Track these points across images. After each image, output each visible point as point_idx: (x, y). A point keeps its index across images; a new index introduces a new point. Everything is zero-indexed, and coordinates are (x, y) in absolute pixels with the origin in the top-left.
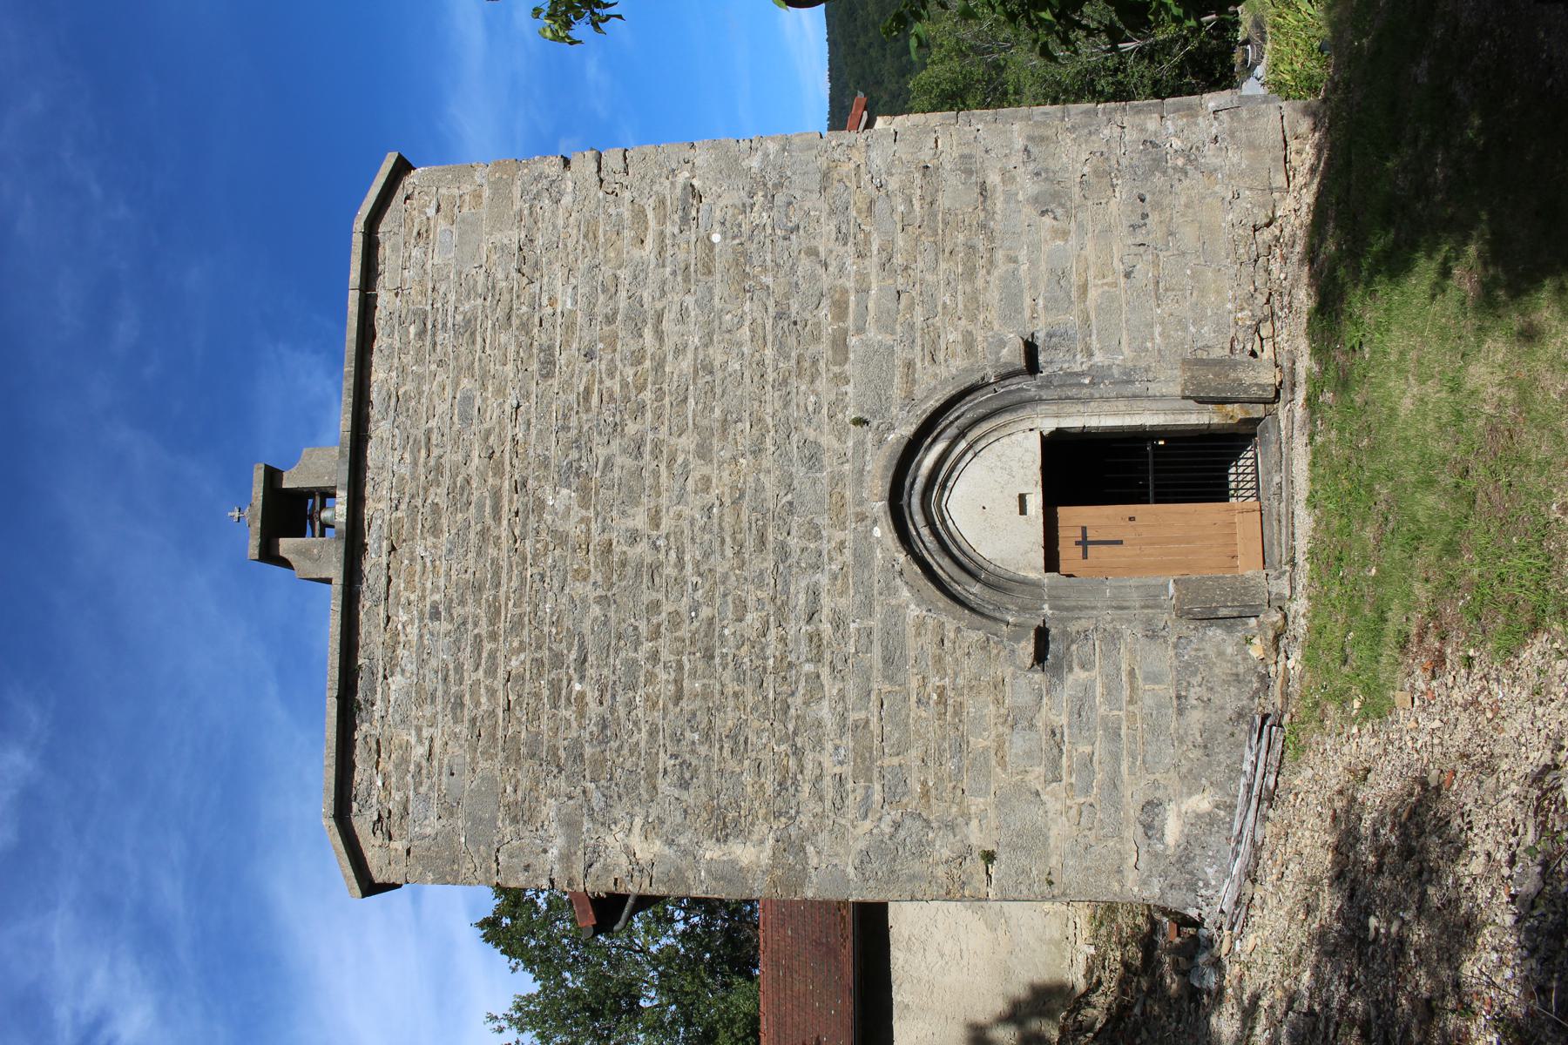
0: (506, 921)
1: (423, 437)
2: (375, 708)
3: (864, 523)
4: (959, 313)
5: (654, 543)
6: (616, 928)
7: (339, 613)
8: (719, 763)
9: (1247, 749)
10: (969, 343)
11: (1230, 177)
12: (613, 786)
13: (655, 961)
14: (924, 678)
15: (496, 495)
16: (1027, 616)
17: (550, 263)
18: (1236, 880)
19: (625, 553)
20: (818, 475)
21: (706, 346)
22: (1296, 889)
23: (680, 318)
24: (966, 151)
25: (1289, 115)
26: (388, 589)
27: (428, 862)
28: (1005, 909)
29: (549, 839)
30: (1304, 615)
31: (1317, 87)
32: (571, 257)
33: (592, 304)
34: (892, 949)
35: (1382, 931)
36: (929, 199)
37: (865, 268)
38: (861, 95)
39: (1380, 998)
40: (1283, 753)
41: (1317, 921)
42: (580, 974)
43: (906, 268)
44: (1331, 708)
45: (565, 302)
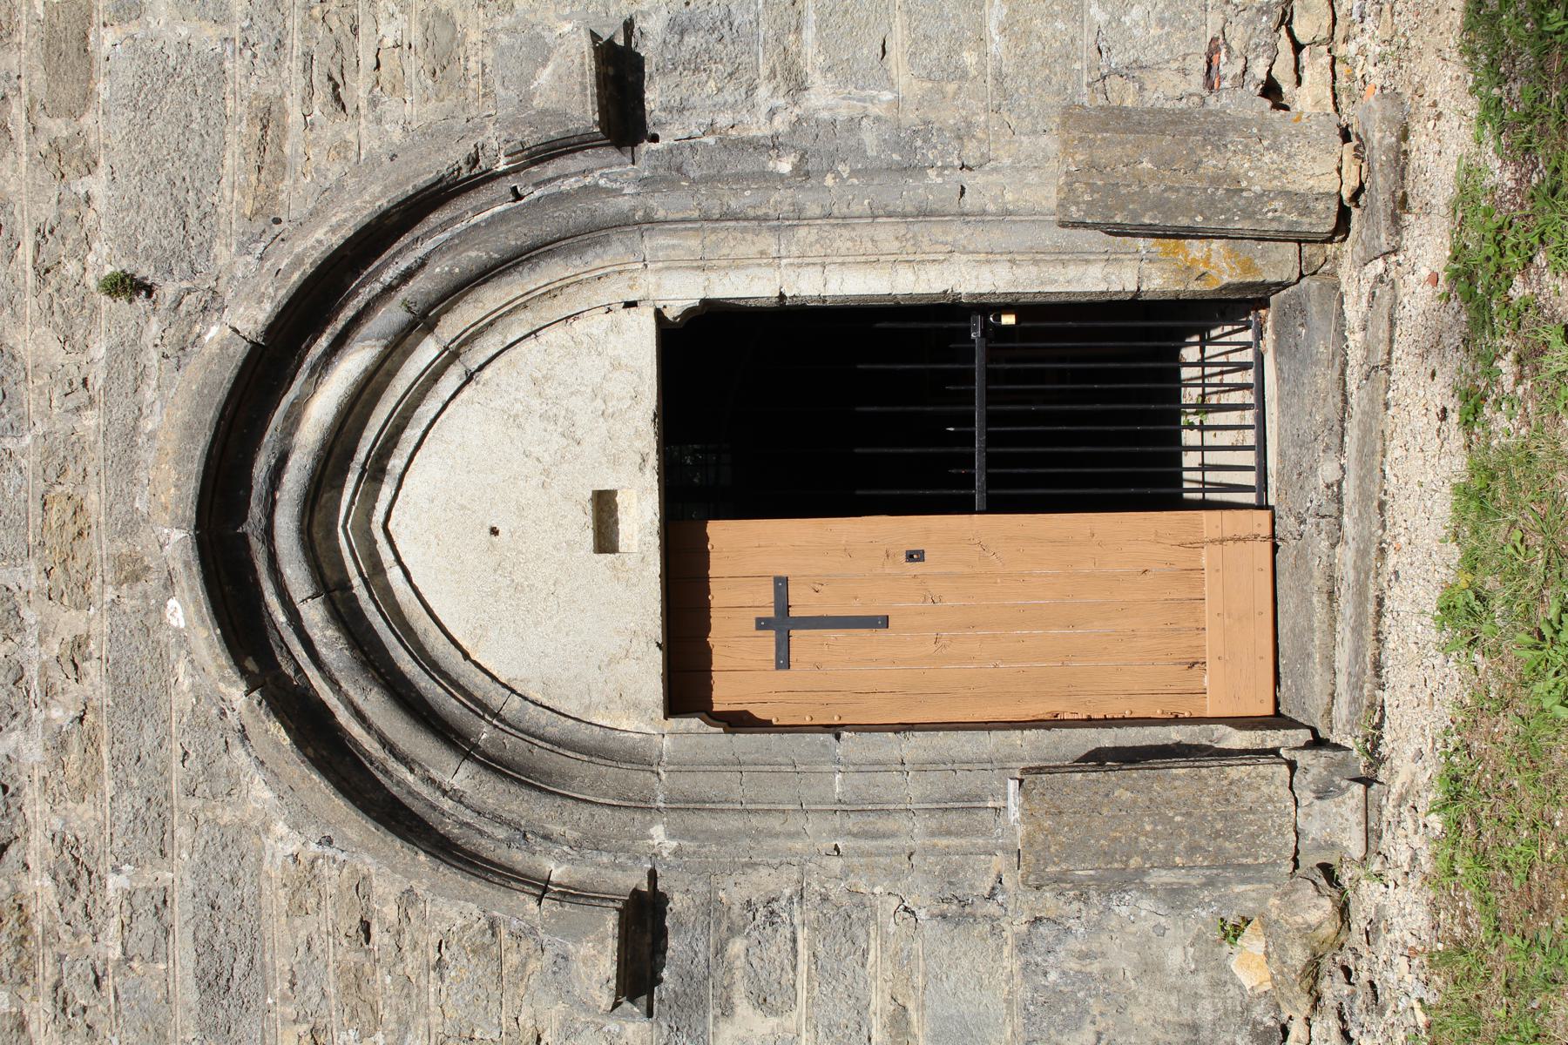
14: (313, 1031)
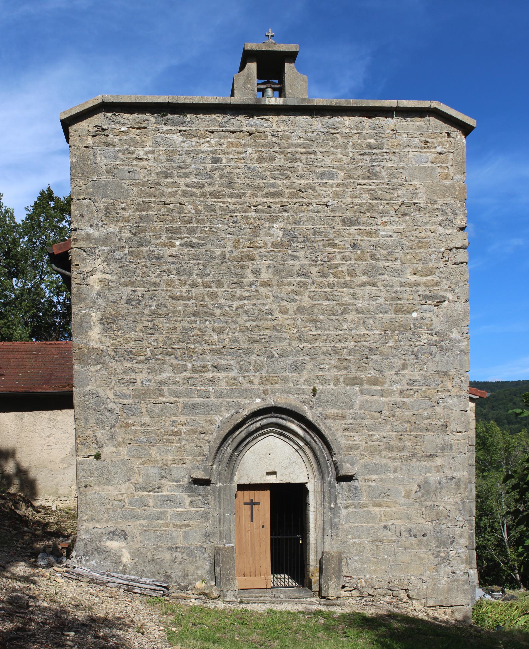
0: (52, 204)
1: (312, 150)
4: (369, 443)
5: (253, 284)
6: (53, 265)
8: (141, 320)
9: (152, 580)
10: (353, 447)
11: (434, 579)
12: (127, 263)
13: (37, 286)
14: (185, 424)
15: (279, 195)
17: (406, 221)
18: (90, 574)
19: (248, 268)
20: (287, 370)
21: (357, 310)
22: (86, 601)
24: (454, 448)
25: (464, 609)
27: (81, 158)
28: (72, 467)
29: (97, 228)
30: (216, 607)
31: (478, 623)
32: (409, 233)
33: (382, 246)
34: (50, 411)
35: (68, 638)
36: (429, 428)
38: (488, 395)
39: (37, 636)
40: (151, 596)
41: (72, 610)
42: (27, 245)
43: (393, 416)
44: (172, 618)
45: (384, 231)
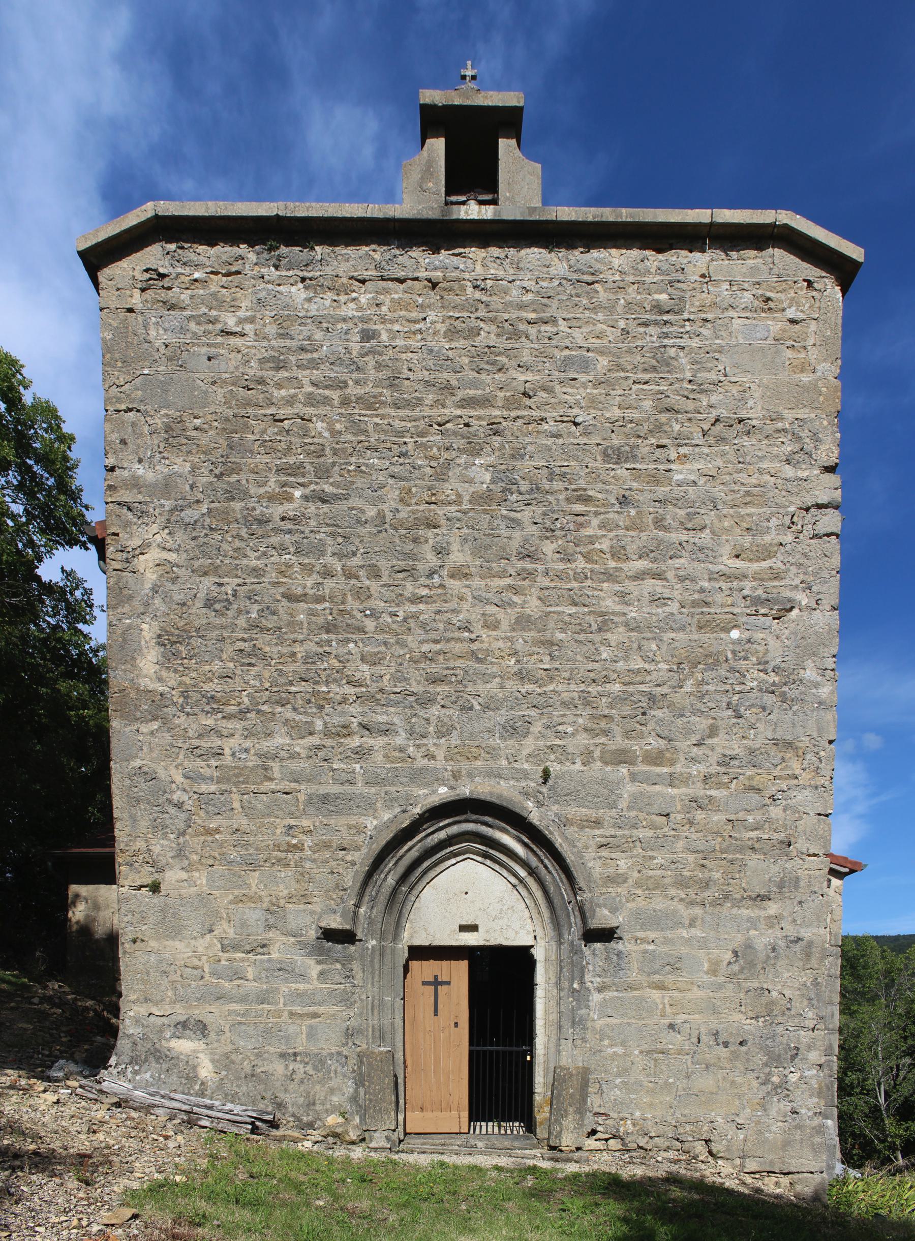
1: (549, 315)
2: (273, 269)
3: (451, 778)
4: (644, 871)
7: (364, 215)
10: (615, 880)
11: (758, 1123)
12: (205, 531)
14: (311, 831)
15: (485, 402)
16: (366, 926)
19: (427, 542)
20: (497, 735)
21: (627, 625)
23: (655, 598)
24: (802, 884)
26: (392, 280)
27: (122, 332)
29: (152, 466)
32: (728, 478)
33: (675, 502)
36: (757, 846)
37: (693, 783)
43: (691, 823)
